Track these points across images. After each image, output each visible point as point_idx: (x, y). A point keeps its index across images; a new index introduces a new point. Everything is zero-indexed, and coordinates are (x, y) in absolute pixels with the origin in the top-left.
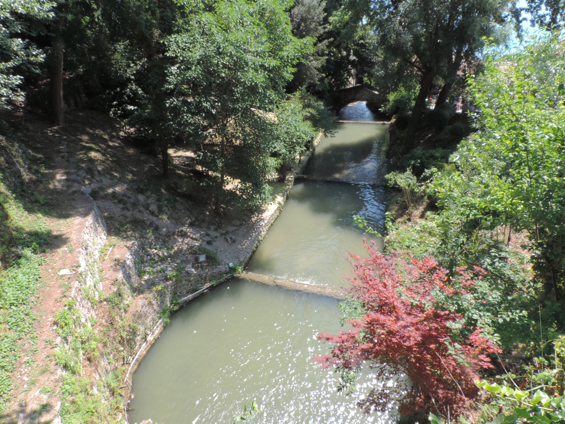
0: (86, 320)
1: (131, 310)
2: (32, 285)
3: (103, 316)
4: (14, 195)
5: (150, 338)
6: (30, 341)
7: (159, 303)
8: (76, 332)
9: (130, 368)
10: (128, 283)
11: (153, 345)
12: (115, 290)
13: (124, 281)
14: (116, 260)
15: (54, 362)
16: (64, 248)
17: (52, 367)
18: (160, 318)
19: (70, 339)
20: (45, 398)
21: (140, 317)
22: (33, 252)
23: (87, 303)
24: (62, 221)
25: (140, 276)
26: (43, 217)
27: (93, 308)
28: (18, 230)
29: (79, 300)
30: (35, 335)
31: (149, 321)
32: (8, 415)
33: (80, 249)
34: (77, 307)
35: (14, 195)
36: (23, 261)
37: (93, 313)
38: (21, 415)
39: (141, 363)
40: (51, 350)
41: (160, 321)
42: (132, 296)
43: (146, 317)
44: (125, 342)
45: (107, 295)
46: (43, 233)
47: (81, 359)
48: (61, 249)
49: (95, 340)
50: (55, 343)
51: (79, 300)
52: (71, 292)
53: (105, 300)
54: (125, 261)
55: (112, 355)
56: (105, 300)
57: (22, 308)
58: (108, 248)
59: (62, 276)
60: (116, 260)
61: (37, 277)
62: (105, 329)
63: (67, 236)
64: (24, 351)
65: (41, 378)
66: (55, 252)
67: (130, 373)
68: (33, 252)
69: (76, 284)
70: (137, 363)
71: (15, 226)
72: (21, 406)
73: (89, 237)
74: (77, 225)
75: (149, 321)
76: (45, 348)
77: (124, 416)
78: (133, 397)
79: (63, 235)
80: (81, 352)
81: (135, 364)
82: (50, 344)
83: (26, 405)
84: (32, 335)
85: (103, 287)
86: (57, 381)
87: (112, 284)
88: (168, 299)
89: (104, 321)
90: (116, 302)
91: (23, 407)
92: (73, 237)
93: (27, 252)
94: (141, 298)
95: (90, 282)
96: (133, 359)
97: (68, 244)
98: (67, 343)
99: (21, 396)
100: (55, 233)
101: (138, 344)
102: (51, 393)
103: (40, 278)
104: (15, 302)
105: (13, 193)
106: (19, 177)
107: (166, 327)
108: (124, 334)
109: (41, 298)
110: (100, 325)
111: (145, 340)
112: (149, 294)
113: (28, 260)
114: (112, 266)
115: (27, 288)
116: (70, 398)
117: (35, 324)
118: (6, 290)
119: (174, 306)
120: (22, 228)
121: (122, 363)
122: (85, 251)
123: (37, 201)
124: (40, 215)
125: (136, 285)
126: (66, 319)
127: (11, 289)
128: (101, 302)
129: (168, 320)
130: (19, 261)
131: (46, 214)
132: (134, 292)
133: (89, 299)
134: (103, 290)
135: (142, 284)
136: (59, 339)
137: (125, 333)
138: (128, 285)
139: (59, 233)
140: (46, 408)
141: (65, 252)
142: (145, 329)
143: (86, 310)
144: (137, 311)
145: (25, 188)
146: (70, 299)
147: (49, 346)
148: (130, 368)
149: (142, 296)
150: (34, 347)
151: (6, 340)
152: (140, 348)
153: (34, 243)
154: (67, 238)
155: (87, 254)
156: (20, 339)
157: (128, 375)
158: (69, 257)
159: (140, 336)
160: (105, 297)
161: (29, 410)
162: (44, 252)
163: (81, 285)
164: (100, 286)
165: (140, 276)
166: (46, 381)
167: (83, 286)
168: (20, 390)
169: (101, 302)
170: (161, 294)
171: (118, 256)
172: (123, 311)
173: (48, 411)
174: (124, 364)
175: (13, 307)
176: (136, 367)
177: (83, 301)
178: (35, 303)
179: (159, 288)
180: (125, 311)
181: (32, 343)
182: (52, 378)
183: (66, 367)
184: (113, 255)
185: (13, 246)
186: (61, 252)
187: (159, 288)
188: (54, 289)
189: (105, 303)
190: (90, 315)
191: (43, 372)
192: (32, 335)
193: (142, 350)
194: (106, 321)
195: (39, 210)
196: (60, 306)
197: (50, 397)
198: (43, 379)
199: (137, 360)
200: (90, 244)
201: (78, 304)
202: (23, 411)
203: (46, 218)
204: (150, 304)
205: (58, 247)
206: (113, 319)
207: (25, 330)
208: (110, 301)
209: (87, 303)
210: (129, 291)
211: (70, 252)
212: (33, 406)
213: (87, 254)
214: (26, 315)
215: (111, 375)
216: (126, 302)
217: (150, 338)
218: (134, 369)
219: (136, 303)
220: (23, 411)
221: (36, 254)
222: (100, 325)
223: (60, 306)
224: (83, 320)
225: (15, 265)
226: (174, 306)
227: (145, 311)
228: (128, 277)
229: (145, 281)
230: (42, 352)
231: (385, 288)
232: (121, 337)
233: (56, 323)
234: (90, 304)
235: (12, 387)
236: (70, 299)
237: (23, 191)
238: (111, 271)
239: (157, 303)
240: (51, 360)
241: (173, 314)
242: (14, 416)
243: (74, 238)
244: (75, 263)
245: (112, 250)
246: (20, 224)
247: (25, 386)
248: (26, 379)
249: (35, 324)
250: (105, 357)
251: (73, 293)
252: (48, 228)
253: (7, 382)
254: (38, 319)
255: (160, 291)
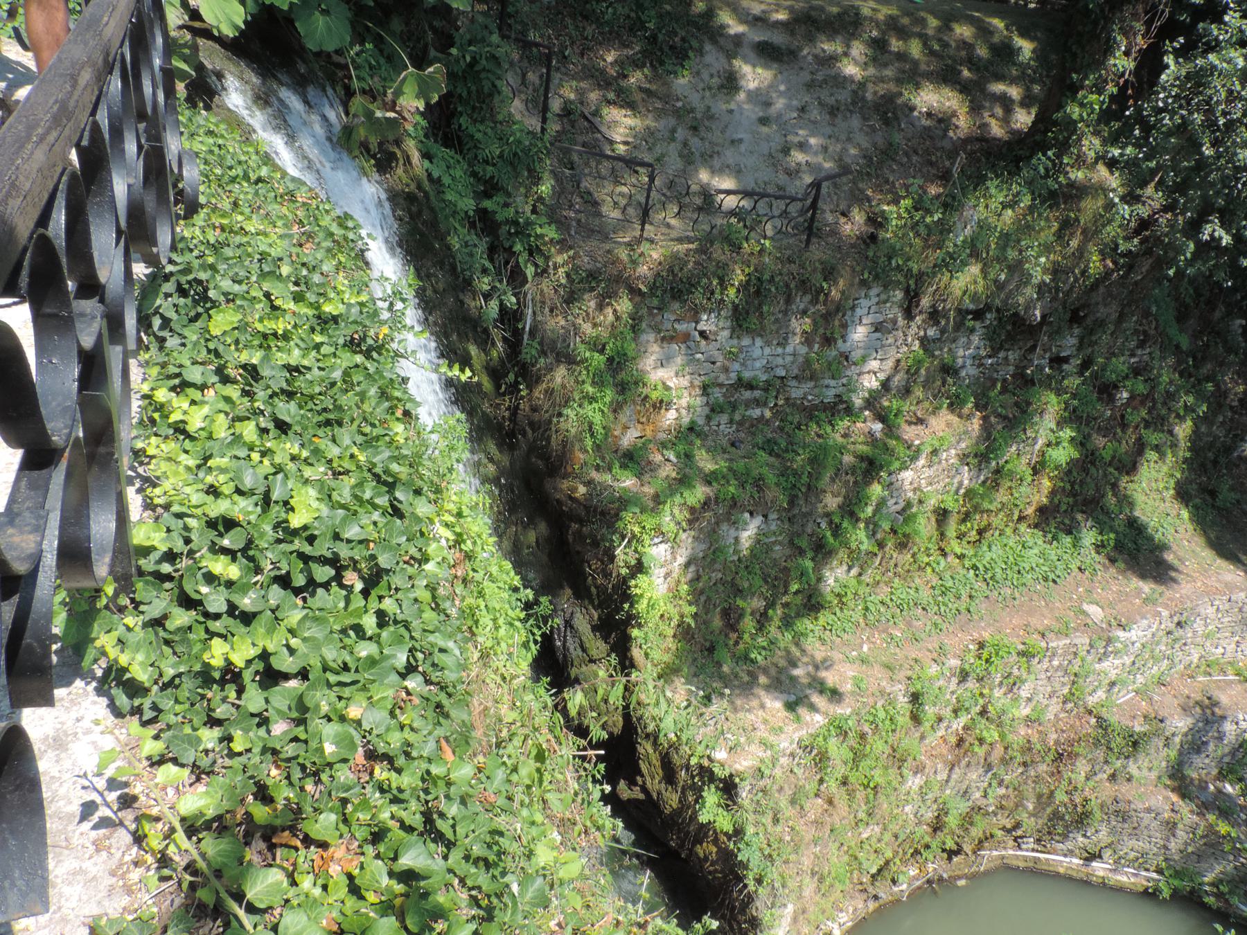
0: (1029, 700)
1: (1124, 789)
2: (1030, 576)
3: (1063, 731)
4: (1188, 455)
5: (1099, 869)
6: (929, 623)
7: (1190, 849)
8: (991, 690)
9: (1011, 852)
10: (1180, 753)
11: (1086, 883)
12: (1137, 729)
13: (1177, 740)
14: (1209, 698)
15: (909, 673)
16: (1147, 587)
17: (901, 675)
18: (1160, 871)
19: (971, 684)
20: (848, 687)
21: (1123, 816)
22: (1098, 546)
23: (1064, 684)
24: (1207, 554)
25: (1221, 776)
26: (1187, 521)
27: (1064, 703)
28: (1126, 501)
29: (1056, 663)
30: (944, 627)
31: (1131, 846)
32: (803, 651)
33: (1165, 613)
34: (1039, 666)
35: (1188, 455)
36: (1067, 540)
37: (1054, 707)
38: (810, 668)
39: (1035, 873)
40: (929, 661)
41: (1155, 875)
42: (1159, 778)
43: (1135, 832)
44: (1049, 810)
45: (1113, 718)
46: (1150, 539)
47: (955, 726)
48: (1141, 583)
49: (1002, 736)
50: (945, 661)
51: (1056, 663)
52: (1058, 639)
53: (1099, 718)
54: (1224, 718)
55: (1002, 791)
56: (1099, 718)
57: (979, 585)
58: (1230, 672)
59: (1084, 613)
60: (1209, 698)
61: (1052, 576)
62: (1038, 747)
63: (1180, 577)
64: (909, 625)
65: (877, 667)
66: (1125, 577)
67: (1003, 857)
68: (1098, 546)
69: (1082, 640)
70: (1031, 864)
71: (1129, 493)
72: (825, 660)
73: (1213, 616)
74: (1219, 581)
75: (1131, 846)
76: (929, 651)
77: (915, 878)
78: (961, 883)
79: (1176, 570)
80: (963, 719)
81: (1025, 859)
82: (940, 655)
83: (827, 668)
84: (940, 621)
85: (1126, 702)
86: (882, 692)
87: (1145, 717)
88: (1218, 868)
89: (1055, 736)
90: (1113, 745)
91: (826, 664)
92: (1185, 588)
93: (1089, 537)
94: (1166, 798)
95: (1111, 667)
96: (1033, 850)
97: (1162, 588)
98: (960, 682)
99: (836, 656)
100: (1169, 557)
101: (1070, 845)
102: (859, 690)
103: (1054, 581)
104: (981, 568)
105: (1190, 449)
106: (1236, 436)
107: (1150, 895)
108: (1061, 797)
109: (1016, 603)
110: (1040, 732)
111: (1086, 859)
112: (1192, 812)
113: (1074, 546)
114: (1188, 697)
115: (1019, 572)
116: (867, 728)
117: (964, 616)
118: (994, 548)
119: (1214, 894)
120: (1131, 505)
121: (1009, 826)
122: (1172, 626)
123: (1213, 493)
124: (1185, 514)
125: (1195, 775)
126: (997, 654)
127: (1000, 552)
128: (1090, 712)
129: (1166, 893)
130: (1062, 536)
131: (1200, 520)
132: (1171, 777)
133: (1074, 683)
134: (1124, 707)
135: (1207, 788)
136: (954, 662)
137: (1066, 799)
138: (1173, 754)
139: (1176, 563)
140: (835, 695)
141: (1139, 591)
142: (1109, 846)
143: (1049, 689)
144: (1130, 802)
145: (1222, 460)
146: (1044, 644)
147: (935, 655)
148: (1011, 852)
149: (1174, 798)
150: (923, 635)
151: (912, 592)
152: (1065, 856)
153: (1112, 536)
154: (1174, 580)
155: (1169, 633)
156: (924, 609)
157: (995, 853)
158: (1133, 605)
159: (1086, 841)
160: (1105, 716)
161: (823, 674)
162: (1113, 561)
163: (1088, 652)
164: (1124, 697)
165: (1221, 776)
166: (877, 678)
167: (1089, 658)
168: (845, 649)
169: (1090, 712)
170: (1212, 846)
171: (1224, 699)
172: (1109, 770)
173: (830, 700)
174: (1009, 831)
175: (972, 572)
176: (1022, 864)
177: (1060, 674)
178: (1000, 599)
179: (1223, 828)
180: (1113, 777)
181: (928, 628)
182: (884, 683)
183: (915, 698)
184: (1219, 688)
185: (1083, 512)
186: (1132, 586)
187: (1223, 828)
188: (1045, 612)
189: (1093, 721)
190: (1045, 702)
191: (888, 667)
192: (940, 621)
193: (1064, 861)
194: (1057, 742)
195: (1196, 507)
196: (1018, 636)
197: (853, 693)
198: (878, 672)
199: (1036, 860)
200: (1198, 625)
201: (1045, 665)
202: (817, 668)
203: (1190, 527)
204: (1171, 826)
205: (1143, 577)
206: (1073, 756)
207: (943, 609)
208: (1106, 730)
209: (1064, 684)
210: (1164, 764)
211: (1146, 600)
212: (830, 678)
213: (1169, 633)
214: (970, 597)
215: (964, 807)
216: (1133, 768)
217: (1099, 869)
218: (1015, 863)
219: (1146, 787)
220: (817, 668)
221: (1098, 553)
222: (1040, 732)
223: (1018, 636)
224: (1024, 693)
225: (1050, 536)
226: (1214, 894)
227: (1145, 822)
228: (1194, 745)
229: (1220, 791)
230: (920, 650)
231: (615, 411)
232: (1052, 793)
233: (981, 645)
234: (1066, 691)
235: (845, 637)
236: (1044, 644)
237: (1215, 462)
238: (1176, 702)
239: (1186, 844)
240: (911, 668)
241: (1189, 900)
242: (805, 659)
243: (1183, 592)
244: (1128, 619)
245: (1232, 682)
246: (1139, 498)
247: (854, 653)
248: (865, 648)
249: (964, 616)
250: (989, 775)
251: (1059, 643)
252: (1170, 538)
253: (848, 626)
254: (975, 617)
255: (1216, 833)
